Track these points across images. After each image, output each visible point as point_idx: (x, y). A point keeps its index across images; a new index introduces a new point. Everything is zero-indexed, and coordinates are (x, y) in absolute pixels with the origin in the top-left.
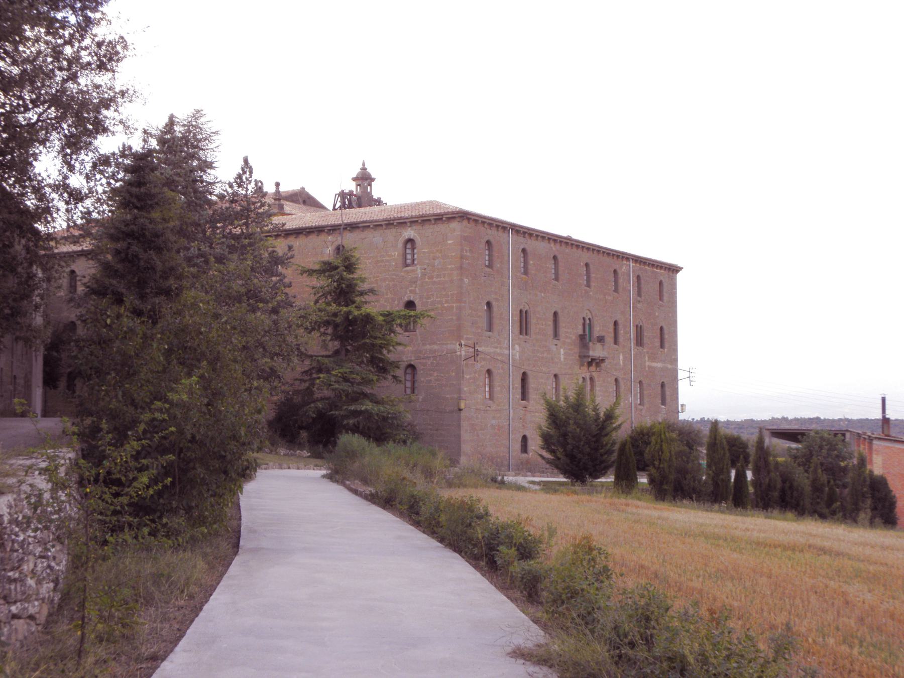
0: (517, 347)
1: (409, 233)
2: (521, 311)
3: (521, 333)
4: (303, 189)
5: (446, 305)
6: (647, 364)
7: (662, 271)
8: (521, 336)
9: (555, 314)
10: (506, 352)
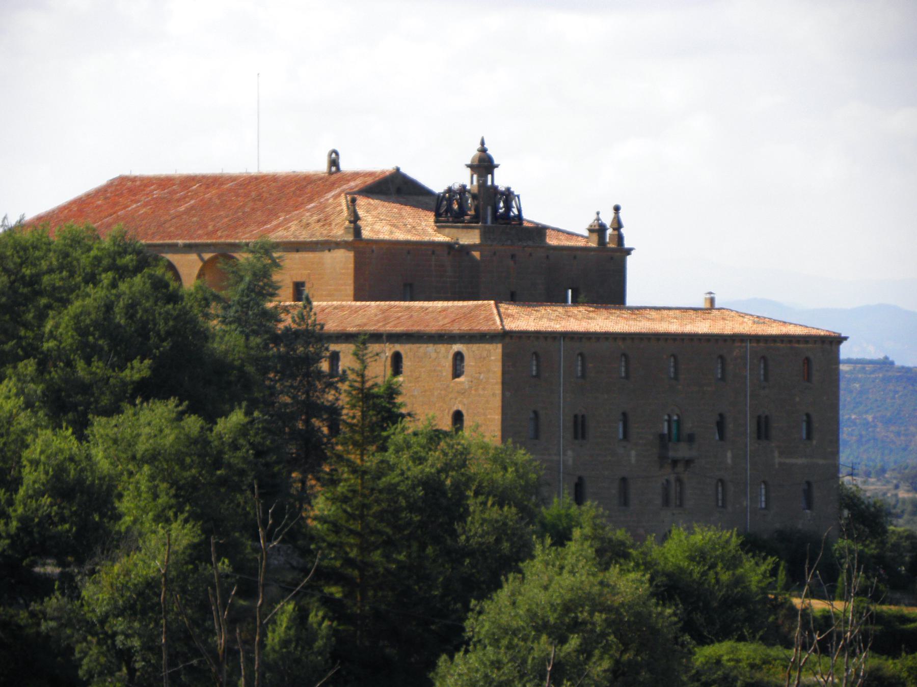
0: (570, 453)
1: (457, 347)
2: (576, 416)
3: (576, 437)
4: (398, 169)
5: (489, 417)
6: (777, 460)
7: (810, 345)
8: (577, 442)
9: (624, 415)
10: (555, 458)
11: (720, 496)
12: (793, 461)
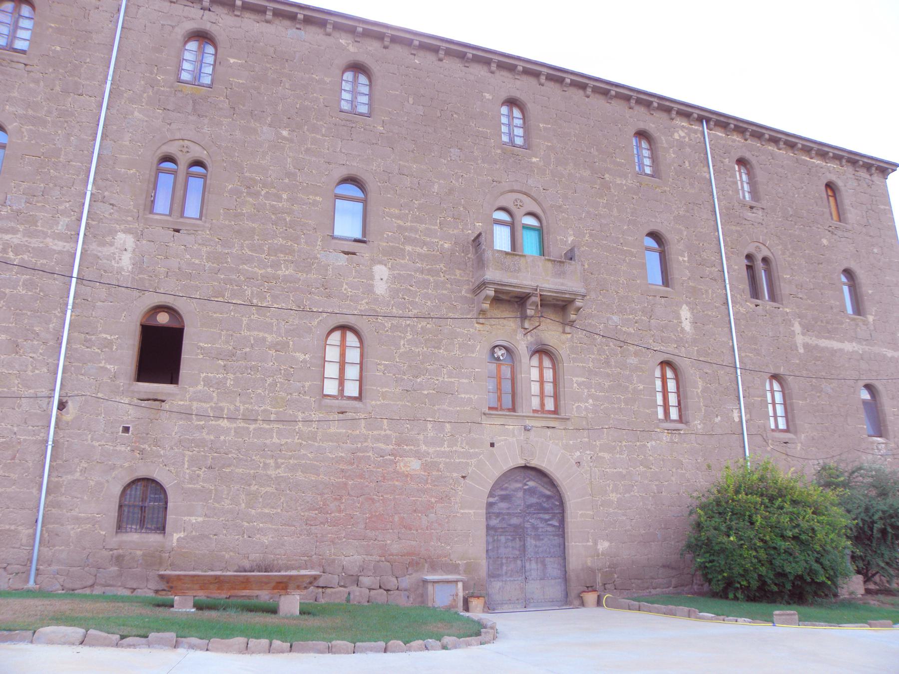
6: (800, 340)
9: (247, 649)
11: (673, 399)
12: (835, 345)
